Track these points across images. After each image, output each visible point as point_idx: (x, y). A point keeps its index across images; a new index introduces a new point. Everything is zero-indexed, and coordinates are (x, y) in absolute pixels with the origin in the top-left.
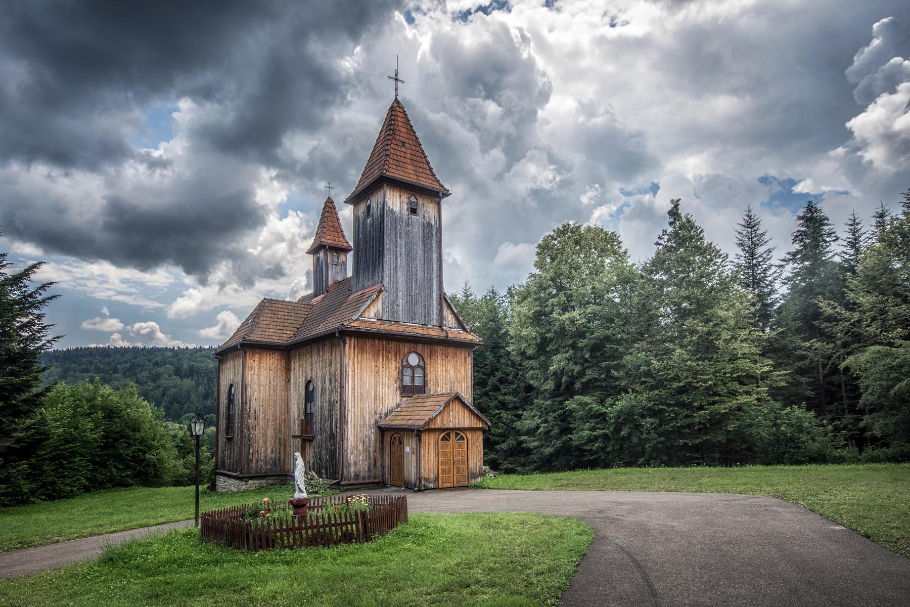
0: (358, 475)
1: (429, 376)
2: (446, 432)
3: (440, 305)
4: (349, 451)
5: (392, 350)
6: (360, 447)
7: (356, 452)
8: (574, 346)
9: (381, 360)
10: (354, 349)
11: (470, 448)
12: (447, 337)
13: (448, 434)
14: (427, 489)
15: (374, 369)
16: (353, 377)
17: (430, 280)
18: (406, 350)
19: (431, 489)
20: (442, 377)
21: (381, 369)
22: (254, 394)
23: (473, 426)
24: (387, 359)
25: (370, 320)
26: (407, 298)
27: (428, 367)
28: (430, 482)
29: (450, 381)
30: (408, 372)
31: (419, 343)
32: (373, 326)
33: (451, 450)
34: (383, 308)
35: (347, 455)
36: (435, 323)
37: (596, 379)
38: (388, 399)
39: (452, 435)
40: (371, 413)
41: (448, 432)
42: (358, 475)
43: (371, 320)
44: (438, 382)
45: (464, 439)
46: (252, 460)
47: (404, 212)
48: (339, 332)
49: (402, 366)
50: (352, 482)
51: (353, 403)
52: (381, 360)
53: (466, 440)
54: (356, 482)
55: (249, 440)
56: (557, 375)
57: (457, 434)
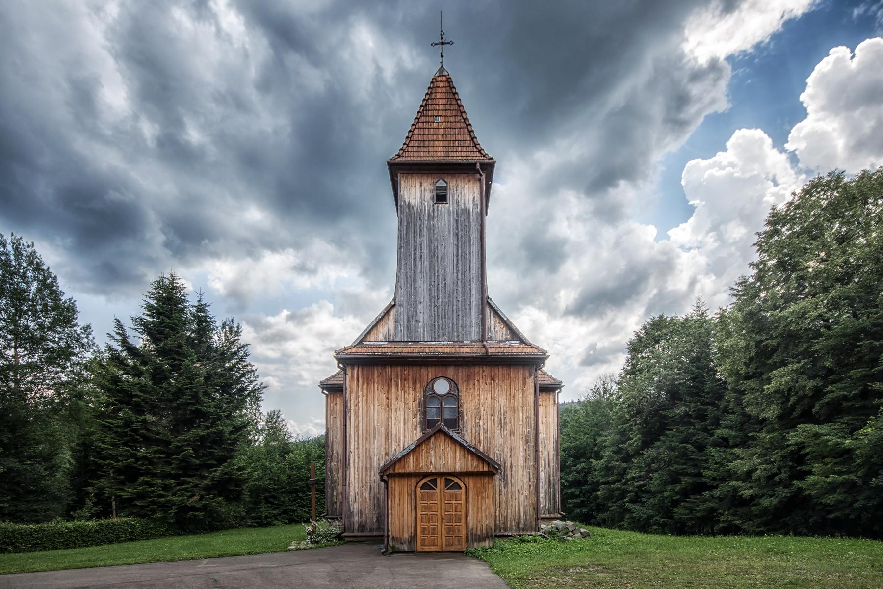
0: (364, 526)
1: (465, 406)
2: (429, 478)
3: (483, 312)
4: (352, 497)
5: (410, 377)
6: (367, 494)
7: (360, 499)
8: (806, 354)
9: (394, 390)
10: (358, 380)
11: (471, 499)
12: (487, 353)
13: (434, 482)
14: (396, 551)
15: (384, 401)
16: (356, 413)
17: (467, 284)
18: (430, 375)
19: (404, 552)
20: (485, 406)
21: (394, 402)
22: (336, 437)
23: (470, 470)
24: (403, 388)
25: (377, 343)
26: (430, 310)
27: (463, 395)
28: (402, 544)
29: (500, 411)
31: (449, 365)
32: (385, 350)
33: (439, 502)
34: (396, 327)
35: (349, 502)
36: (474, 337)
37: (845, 398)
38: (405, 437)
39: (440, 482)
40: (380, 453)
41: (434, 477)
42: (364, 526)
43: (379, 343)
44: (479, 412)
45: (460, 488)
46: (336, 502)
47: (426, 203)
49: (425, 396)
50: (356, 533)
51: (356, 443)
52: (394, 390)
53: (463, 490)
54: (360, 534)
55: (332, 483)
56: (783, 395)
57: (448, 481)
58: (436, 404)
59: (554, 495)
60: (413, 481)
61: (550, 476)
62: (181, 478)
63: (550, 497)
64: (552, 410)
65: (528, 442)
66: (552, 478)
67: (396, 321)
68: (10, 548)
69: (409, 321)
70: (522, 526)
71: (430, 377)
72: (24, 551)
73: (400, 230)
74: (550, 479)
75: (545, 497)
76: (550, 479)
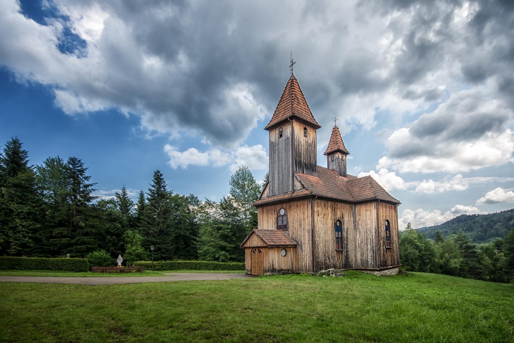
13: (255, 250)
16: (260, 225)
30: (280, 219)
31: (284, 203)
45: (261, 252)
48: (318, 196)
57: (259, 250)
58: (281, 218)
59: (376, 258)
60: (251, 250)
61: (373, 247)
62: (69, 248)
63: (373, 259)
64: (373, 212)
65: (309, 232)
66: (374, 248)
67: (269, 189)
68: (216, 269)
69: (272, 188)
70: (307, 269)
71: (279, 209)
72: (219, 270)
73: (270, 153)
74: (373, 249)
75: (371, 258)
76: (373, 249)
